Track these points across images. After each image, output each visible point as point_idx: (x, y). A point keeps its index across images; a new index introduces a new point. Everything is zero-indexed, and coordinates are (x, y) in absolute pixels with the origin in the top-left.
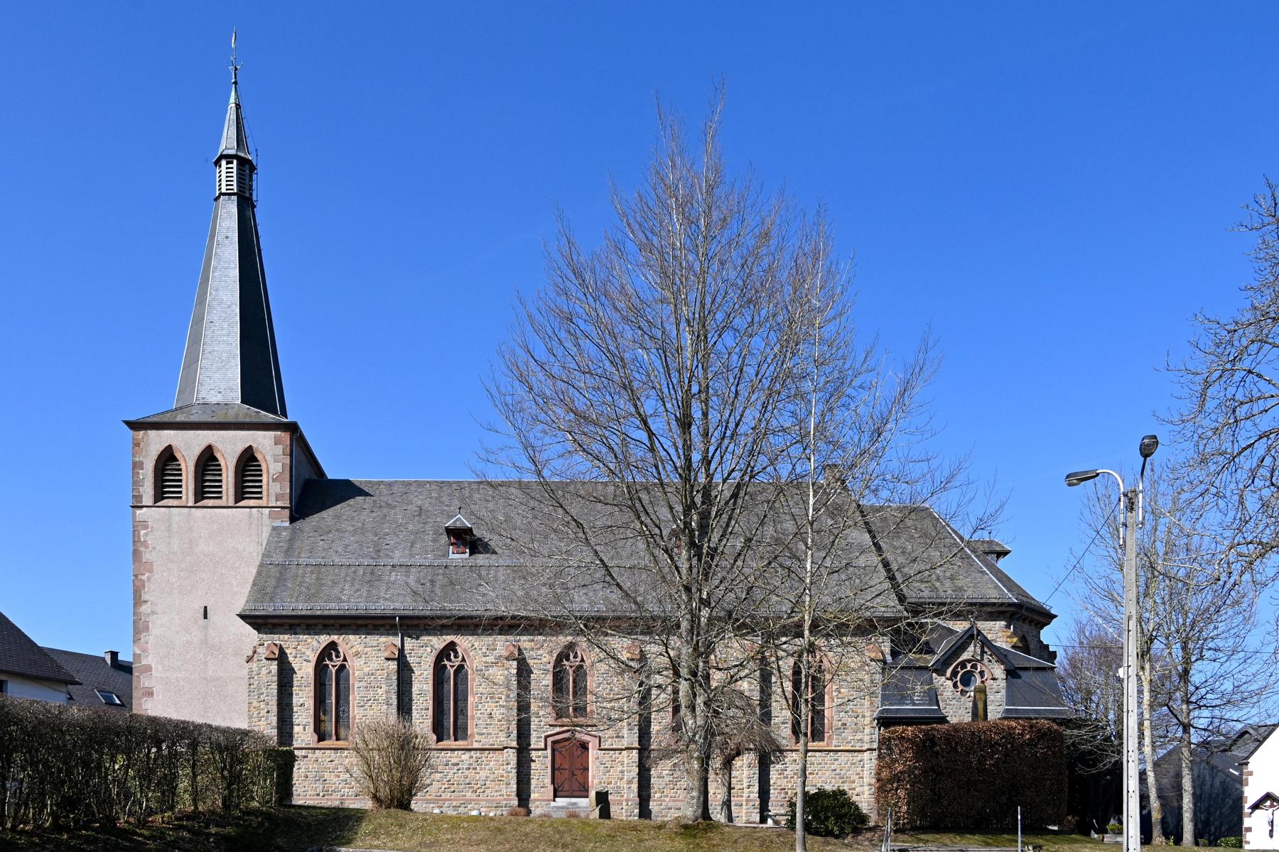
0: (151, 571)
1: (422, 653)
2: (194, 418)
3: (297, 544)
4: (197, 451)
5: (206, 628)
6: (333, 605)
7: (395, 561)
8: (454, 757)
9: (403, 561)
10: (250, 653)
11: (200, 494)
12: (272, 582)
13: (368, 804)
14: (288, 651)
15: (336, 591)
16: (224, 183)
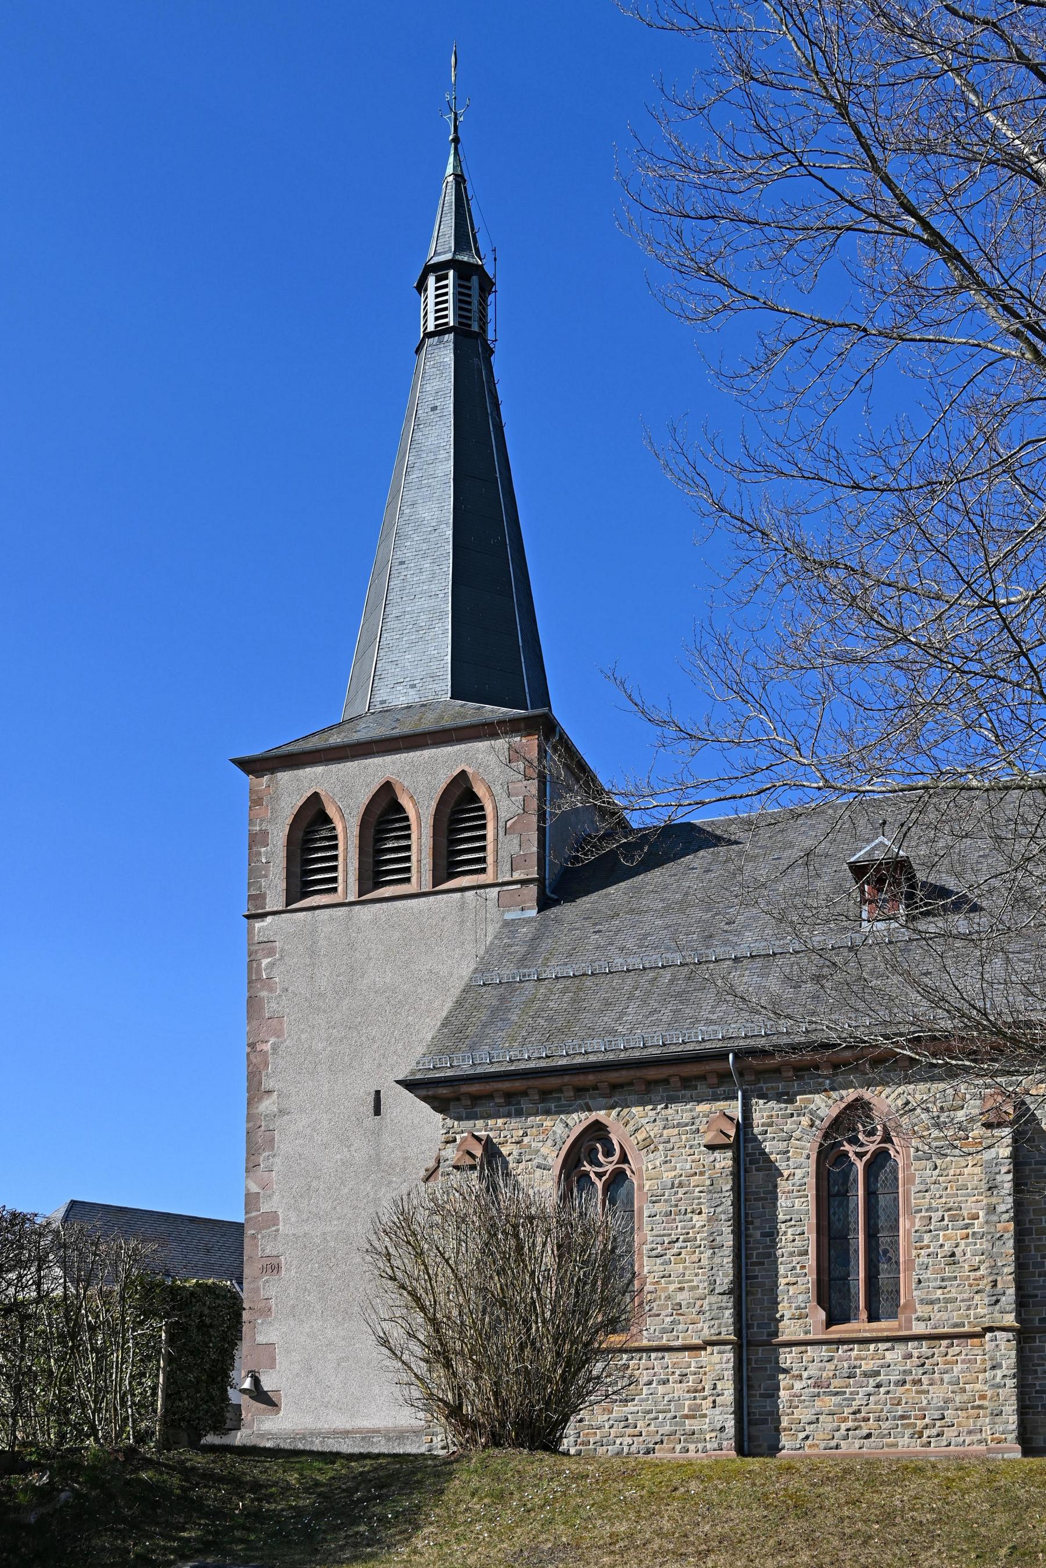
0: (279, 1034)
1: (792, 1133)
2: (364, 732)
3: (546, 944)
4: (364, 798)
5: (377, 1133)
6: (597, 1044)
7: (743, 950)
8: (867, 1358)
9: (759, 947)
10: (432, 1164)
11: (373, 876)
12: (484, 1016)
13: (437, 1440)
14: (504, 1150)
15: (608, 1019)
16: (431, 316)
